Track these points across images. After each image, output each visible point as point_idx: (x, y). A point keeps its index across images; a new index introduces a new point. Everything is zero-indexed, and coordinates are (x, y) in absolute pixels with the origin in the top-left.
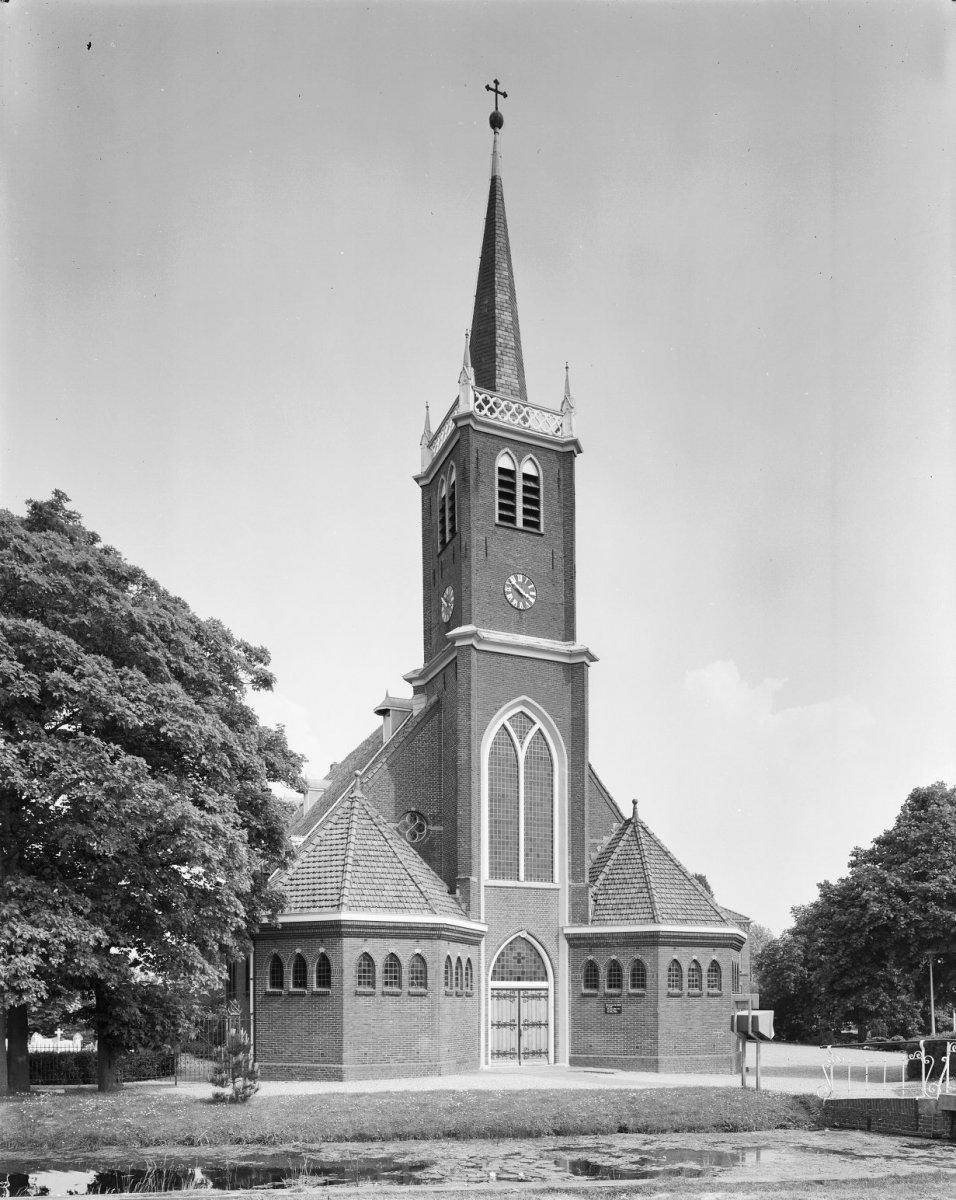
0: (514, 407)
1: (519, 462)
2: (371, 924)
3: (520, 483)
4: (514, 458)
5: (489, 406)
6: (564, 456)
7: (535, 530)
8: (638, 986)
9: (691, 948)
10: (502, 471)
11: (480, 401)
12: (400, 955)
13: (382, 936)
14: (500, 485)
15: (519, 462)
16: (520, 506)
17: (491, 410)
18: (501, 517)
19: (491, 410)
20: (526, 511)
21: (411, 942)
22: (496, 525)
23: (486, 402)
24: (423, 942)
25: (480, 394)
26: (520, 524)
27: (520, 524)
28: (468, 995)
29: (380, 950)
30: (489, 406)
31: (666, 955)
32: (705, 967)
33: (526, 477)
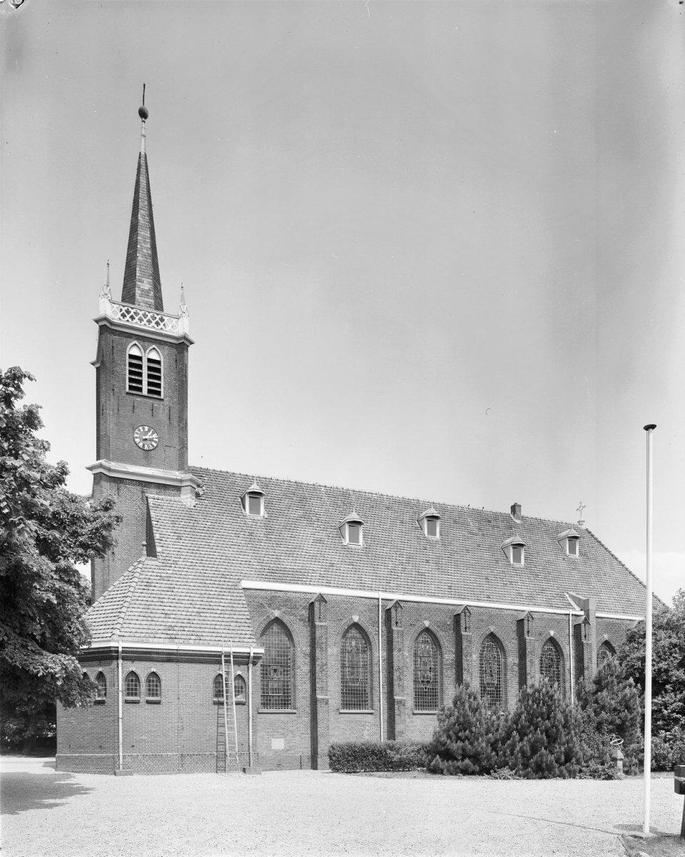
0: (149, 315)
1: (145, 351)
2: (195, 652)
3: (145, 364)
4: (141, 348)
5: (130, 314)
6: (181, 346)
7: (158, 397)
8: (132, 695)
9: (190, 665)
10: (131, 357)
11: (162, 324)
12: (138, 672)
13: (201, 662)
14: (160, 377)
15: (145, 351)
16: (145, 379)
17: (132, 318)
18: (131, 388)
19: (132, 318)
20: (150, 384)
21: (148, 664)
22: (127, 393)
23: (128, 312)
24: (136, 663)
25: (149, 313)
26: (145, 392)
27: (145, 392)
28: (102, 703)
29: (143, 669)
30: (130, 314)
31: (123, 668)
32: (143, 679)
33: (150, 360)
